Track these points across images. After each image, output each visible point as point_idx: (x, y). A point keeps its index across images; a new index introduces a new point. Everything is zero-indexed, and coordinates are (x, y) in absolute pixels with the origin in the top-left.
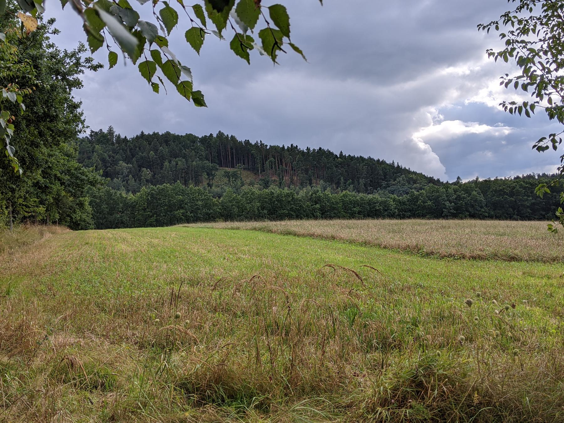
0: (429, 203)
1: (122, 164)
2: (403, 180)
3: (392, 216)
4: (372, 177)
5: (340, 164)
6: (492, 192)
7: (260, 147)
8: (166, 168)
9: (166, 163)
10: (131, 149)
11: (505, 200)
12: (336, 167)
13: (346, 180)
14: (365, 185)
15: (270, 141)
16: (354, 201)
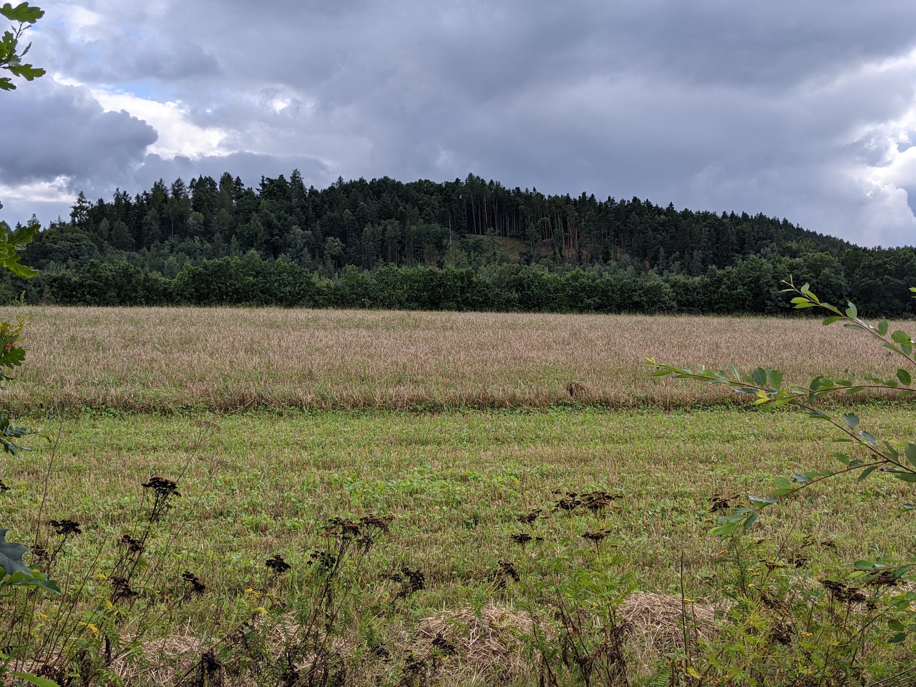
0: (740, 289)
1: (297, 230)
2: (773, 251)
3: (667, 310)
4: (717, 248)
5: (662, 225)
6: (863, 268)
7: (533, 200)
8: (366, 237)
9: (368, 229)
10: (317, 206)
11: (885, 284)
12: (655, 230)
13: (669, 253)
14: (703, 261)
15: (550, 188)
16: (590, 286)
